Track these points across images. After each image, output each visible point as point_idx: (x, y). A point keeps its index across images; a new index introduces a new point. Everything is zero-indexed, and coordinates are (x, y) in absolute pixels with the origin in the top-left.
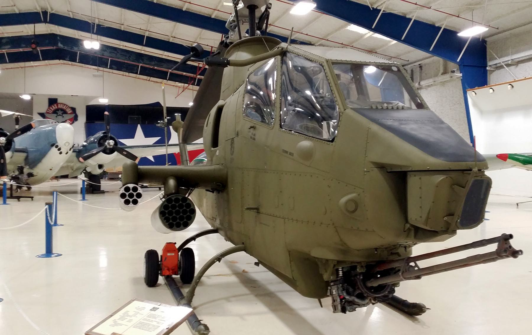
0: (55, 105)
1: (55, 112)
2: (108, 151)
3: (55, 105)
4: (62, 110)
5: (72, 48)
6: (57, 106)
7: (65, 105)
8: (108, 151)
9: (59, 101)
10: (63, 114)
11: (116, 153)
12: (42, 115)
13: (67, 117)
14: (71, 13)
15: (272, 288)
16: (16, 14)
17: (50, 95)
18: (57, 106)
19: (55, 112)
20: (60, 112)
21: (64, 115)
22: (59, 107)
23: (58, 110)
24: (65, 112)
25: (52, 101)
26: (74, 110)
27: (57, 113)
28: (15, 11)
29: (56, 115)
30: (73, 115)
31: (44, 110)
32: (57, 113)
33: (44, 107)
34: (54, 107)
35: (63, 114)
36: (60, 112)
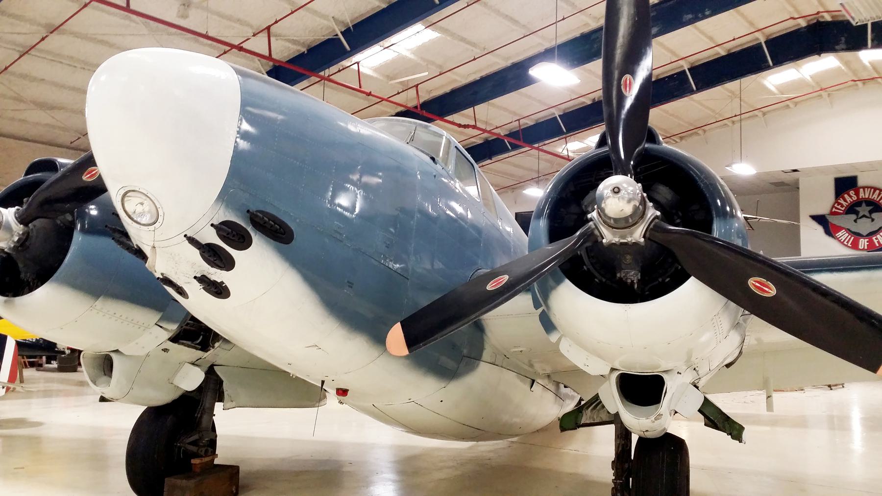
0: (852, 193)
1: (851, 209)
2: (633, 276)
3: (852, 193)
4: (869, 202)
5: (347, 124)
6: (857, 194)
7: (875, 189)
8: (633, 276)
9: (861, 182)
10: (871, 212)
11: (692, 290)
12: (820, 219)
14: (825, 15)
15: (50, 385)
16: (723, 57)
17: (836, 168)
18: (857, 194)
19: (851, 209)
20: (864, 210)
21: (874, 215)
22: (862, 195)
23: (859, 203)
25: (845, 184)
27: (857, 213)
28: (719, 53)
29: (854, 217)
31: (823, 209)
32: (857, 213)
33: (821, 199)
34: (850, 198)
35: (871, 212)
36: (864, 210)
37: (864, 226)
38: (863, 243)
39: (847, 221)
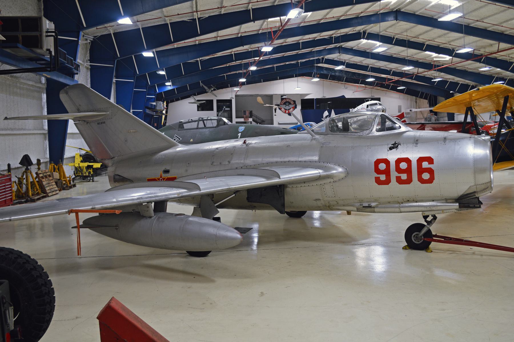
13: (291, 106)
19: (285, 104)
20: (287, 104)
24: (290, 104)
26: (294, 102)
30: (294, 105)
36: (287, 104)
37: (287, 108)
38: (287, 112)
39: (283, 107)
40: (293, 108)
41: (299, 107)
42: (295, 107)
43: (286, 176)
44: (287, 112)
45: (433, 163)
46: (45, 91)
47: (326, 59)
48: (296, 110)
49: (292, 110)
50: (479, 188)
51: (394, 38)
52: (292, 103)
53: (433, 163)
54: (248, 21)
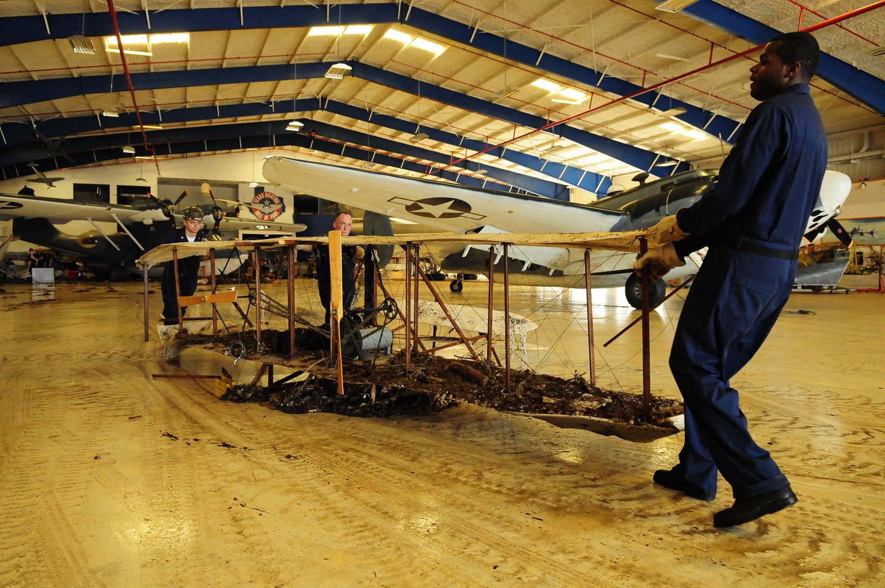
4: (269, 199)
19: (262, 202)
20: (267, 202)
26: (281, 199)
30: (281, 206)
31: (249, 200)
34: (261, 196)
36: (267, 202)
37: (267, 210)
38: (266, 217)
39: (260, 207)
40: (277, 211)
41: (290, 211)
42: (283, 209)
43: (711, 538)
44: (266, 217)
45: (75, 185)
46: (715, 467)
47: (330, 101)
48: (283, 214)
49: (275, 214)
50: (693, 158)
51: (600, 74)
52: (276, 201)
53: (75, 185)
54: (291, 110)
